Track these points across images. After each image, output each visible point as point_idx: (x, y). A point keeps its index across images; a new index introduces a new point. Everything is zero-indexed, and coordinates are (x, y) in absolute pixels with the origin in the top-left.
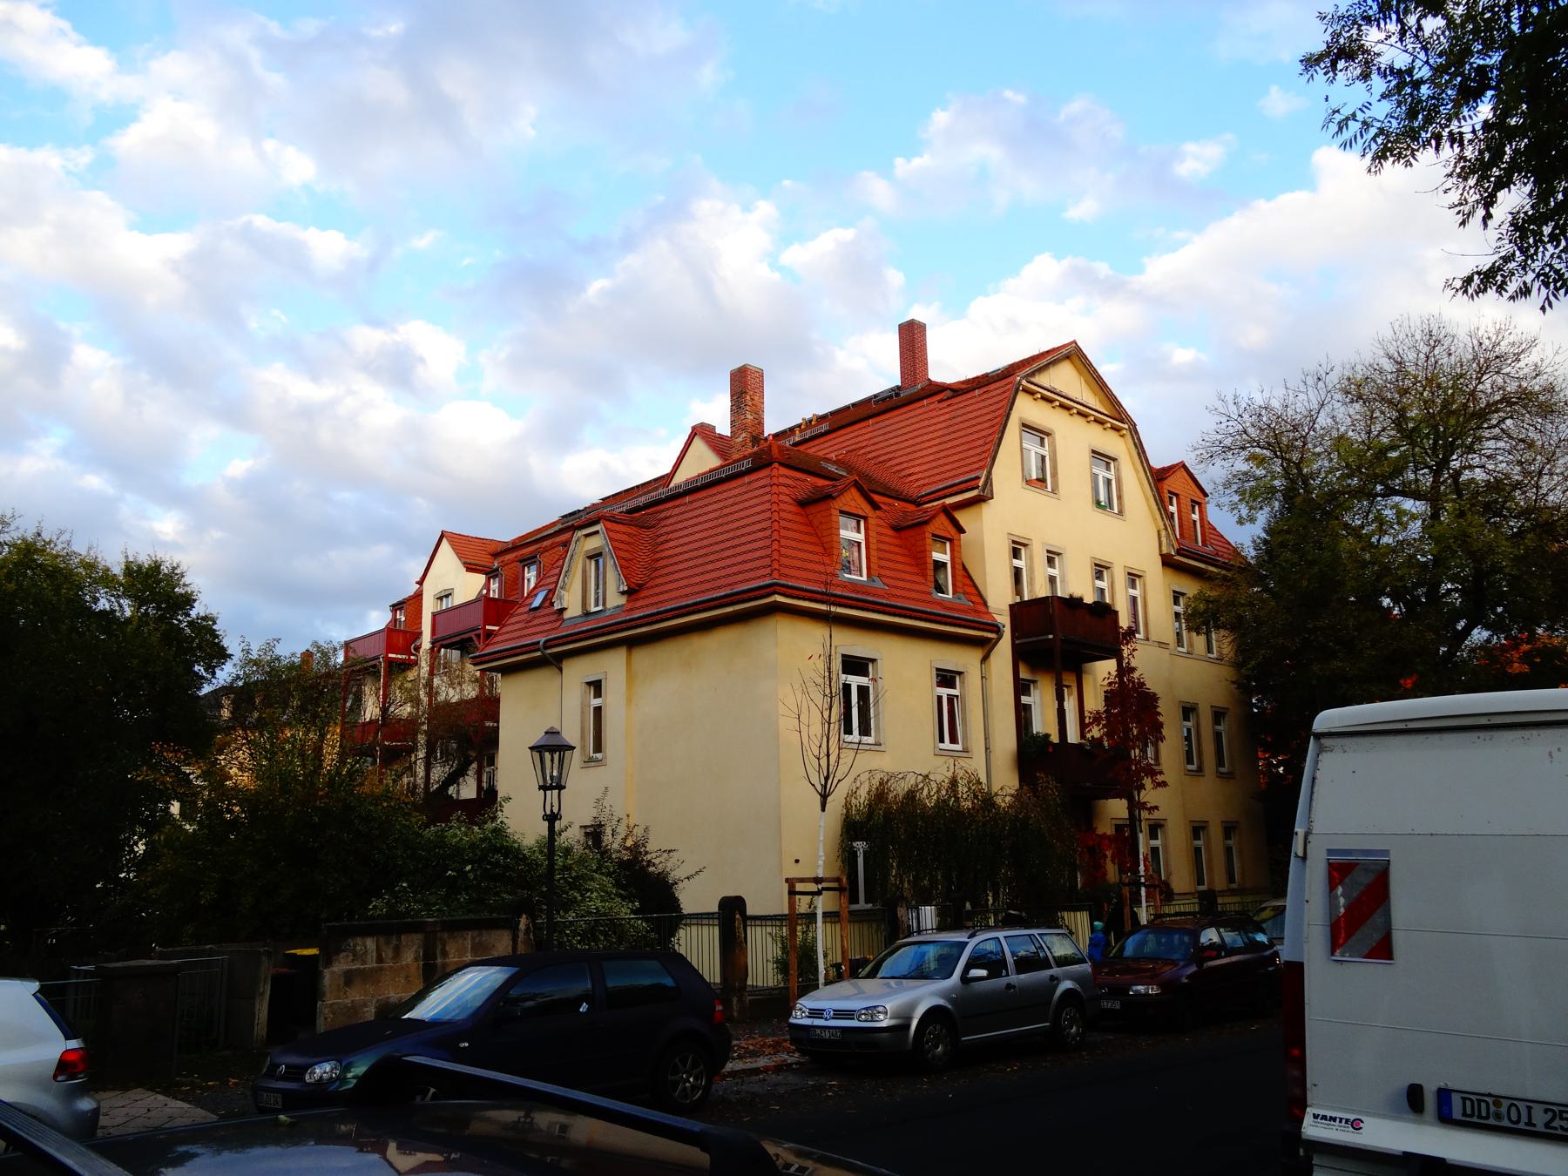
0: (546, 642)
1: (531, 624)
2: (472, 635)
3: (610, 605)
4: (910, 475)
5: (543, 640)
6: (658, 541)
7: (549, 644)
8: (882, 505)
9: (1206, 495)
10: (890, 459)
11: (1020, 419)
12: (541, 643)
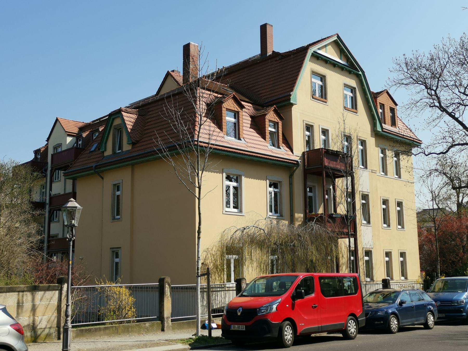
0: (96, 166)
1: (90, 158)
2: (69, 164)
3: (125, 149)
4: (261, 94)
5: (95, 165)
6: (146, 122)
7: (97, 167)
8: (245, 106)
9: (396, 105)
10: (253, 87)
11: (311, 69)
12: (94, 167)
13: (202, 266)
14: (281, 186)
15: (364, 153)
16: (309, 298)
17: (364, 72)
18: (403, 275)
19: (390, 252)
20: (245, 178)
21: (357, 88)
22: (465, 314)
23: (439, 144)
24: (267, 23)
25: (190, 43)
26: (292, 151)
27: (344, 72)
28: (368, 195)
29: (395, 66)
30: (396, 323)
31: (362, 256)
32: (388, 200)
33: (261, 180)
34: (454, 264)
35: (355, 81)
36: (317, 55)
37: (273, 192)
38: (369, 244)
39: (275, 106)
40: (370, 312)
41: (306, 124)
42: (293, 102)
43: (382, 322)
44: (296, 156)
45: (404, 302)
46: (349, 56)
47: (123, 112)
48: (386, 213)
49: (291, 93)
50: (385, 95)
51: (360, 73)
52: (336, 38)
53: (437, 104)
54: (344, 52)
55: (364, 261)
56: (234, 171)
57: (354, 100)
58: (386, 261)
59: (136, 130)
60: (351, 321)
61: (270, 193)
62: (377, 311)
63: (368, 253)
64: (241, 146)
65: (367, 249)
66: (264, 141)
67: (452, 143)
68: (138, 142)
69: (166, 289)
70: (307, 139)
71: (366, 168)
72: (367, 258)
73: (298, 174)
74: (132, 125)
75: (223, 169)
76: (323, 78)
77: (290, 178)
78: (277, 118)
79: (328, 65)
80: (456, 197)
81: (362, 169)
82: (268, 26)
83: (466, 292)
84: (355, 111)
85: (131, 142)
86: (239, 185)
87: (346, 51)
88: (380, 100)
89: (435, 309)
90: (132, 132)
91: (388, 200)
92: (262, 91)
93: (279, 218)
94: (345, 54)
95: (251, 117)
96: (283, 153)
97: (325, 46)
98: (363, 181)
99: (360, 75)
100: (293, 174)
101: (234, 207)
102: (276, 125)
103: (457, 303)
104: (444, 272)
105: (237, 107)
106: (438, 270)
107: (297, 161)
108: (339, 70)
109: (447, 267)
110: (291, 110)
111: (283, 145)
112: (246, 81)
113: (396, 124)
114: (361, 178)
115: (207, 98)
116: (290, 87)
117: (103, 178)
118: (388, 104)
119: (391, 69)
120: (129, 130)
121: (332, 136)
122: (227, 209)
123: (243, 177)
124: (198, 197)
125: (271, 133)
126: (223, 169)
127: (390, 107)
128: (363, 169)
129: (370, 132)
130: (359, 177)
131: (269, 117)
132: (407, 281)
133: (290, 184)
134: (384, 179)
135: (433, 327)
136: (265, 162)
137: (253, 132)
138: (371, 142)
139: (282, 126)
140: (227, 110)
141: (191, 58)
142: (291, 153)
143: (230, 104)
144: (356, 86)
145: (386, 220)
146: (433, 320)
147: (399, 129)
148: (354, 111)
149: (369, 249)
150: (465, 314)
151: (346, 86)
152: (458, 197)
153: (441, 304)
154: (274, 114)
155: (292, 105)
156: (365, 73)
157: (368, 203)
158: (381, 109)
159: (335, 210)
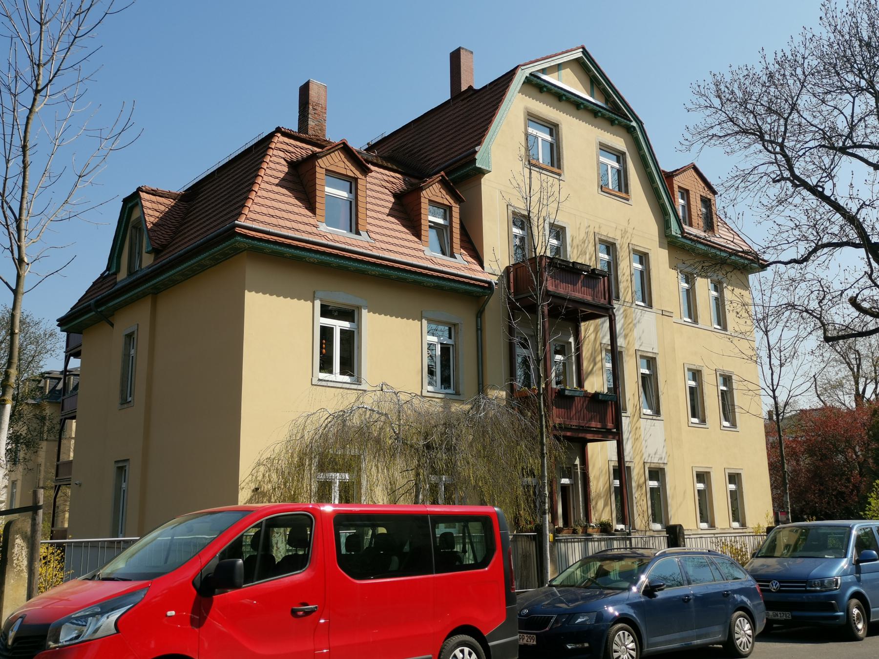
4: (429, 160)
9: (714, 192)
11: (526, 108)
13: (252, 497)
14: (458, 333)
15: (645, 277)
16: (547, 563)
17: (641, 122)
18: (736, 518)
19: (706, 472)
20: (369, 312)
21: (627, 154)
22: (841, 613)
23: (789, 243)
24: (462, 46)
25: (309, 81)
26: (481, 265)
27: (598, 121)
28: (655, 358)
29: (694, 98)
30: (632, 645)
31: (642, 480)
32: (701, 371)
33: (408, 319)
34: (843, 498)
35: (622, 140)
36: (542, 82)
37: (439, 345)
38: (658, 456)
39: (442, 173)
40: (555, 616)
41: (514, 213)
42: (483, 165)
43: (586, 645)
44: (489, 273)
45: (661, 586)
46: (610, 90)
47: (143, 191)
48: (695, 397)
49: (477, 148)
50: (692, 172)
51: (634, 124)
52: (581, 55)
53: (787, 174)
54: (599, 83)
55: (648, 490)
56: (342, 297)
57: (622, 177)
58: (730, 491)
59: (166, 227)
60: (462, 651)
61: (431, 346)
62: (575, 614)
63: (656, 473)
64: (350, 245)
65: (653, 466)
66: (417, 240)
67: (816, 242)
68: (164, 247)
69: (16, 550)
70: (517, 242)
71: (650, 306)
72: (654, 484)
73: (496, 309)
74: (158, 217)
75: (314, 292)
76: (553, 128)
77: (477, 317)
78: (448, 197)
79: (563, 105)
80: (853, 383)
81: (639, 307)
82: (462, 52)
83: (845, 557)
84: (624, 195)
85: (151, 248)
86: (356, 327)
87: (603, 81)
88: (678, 181)
89: (756, 603)
90: (156, 229)
91: (701, 371)
92: (432, 156)
93: (449, 397)
94: (601, 87)
95: (395, 195)
96: (459, 266)
97: (559, 67)
98: (643, 332)
99: (634, 127)
100: (484, 309)
101: (343, 372)
102: (447, 211)
103: (822, 584)
104: (823, 513)
105: (353, 169)
106: (787, 505)
107: (490, 283)
108: (589, 117)
109: (828, 503)
110: (480, 184)
111: (462, 251)
112: (410, 145)
113: (716, 228)
114: (638, 326)
115: (293, 152)
116: (476, 138)
117: (112, 325)
118: (697, 190)
119: (690, 106)
120: (149, 226)
121: (572, 240)
122: (323, 376)
123: (364, 312)
124: (14, 288)
125: (435, 226)
126: (314, 292)
127: (701, 195)
128: (641, 308)
129: (657, 239)
130: (634, 322)
131: (430, 195)
132: (744, 531)
133: (477, 330)
134: (690, 331)
135: (750, 653)
136: (415, 282)
137: (393, 223)
138: (660, 258)
139: (461, 214)
140: (329, 172)
141: (311, 107)
142: (479, 268)
143: (337, 160)
144: (626, 149)
145: (697, 409)
146: (749, 632)
147: (722, 237)
148: (621, 195)
149: (658, 465)
150: (841, 613)
151: (605, 148)
152: (857, 383)
153: (781, 586)
154: (441, 190)
155: (481, 172)
156: (644, 125)
157: (655, 375)
158: (683, 198)
159: (580, 383)
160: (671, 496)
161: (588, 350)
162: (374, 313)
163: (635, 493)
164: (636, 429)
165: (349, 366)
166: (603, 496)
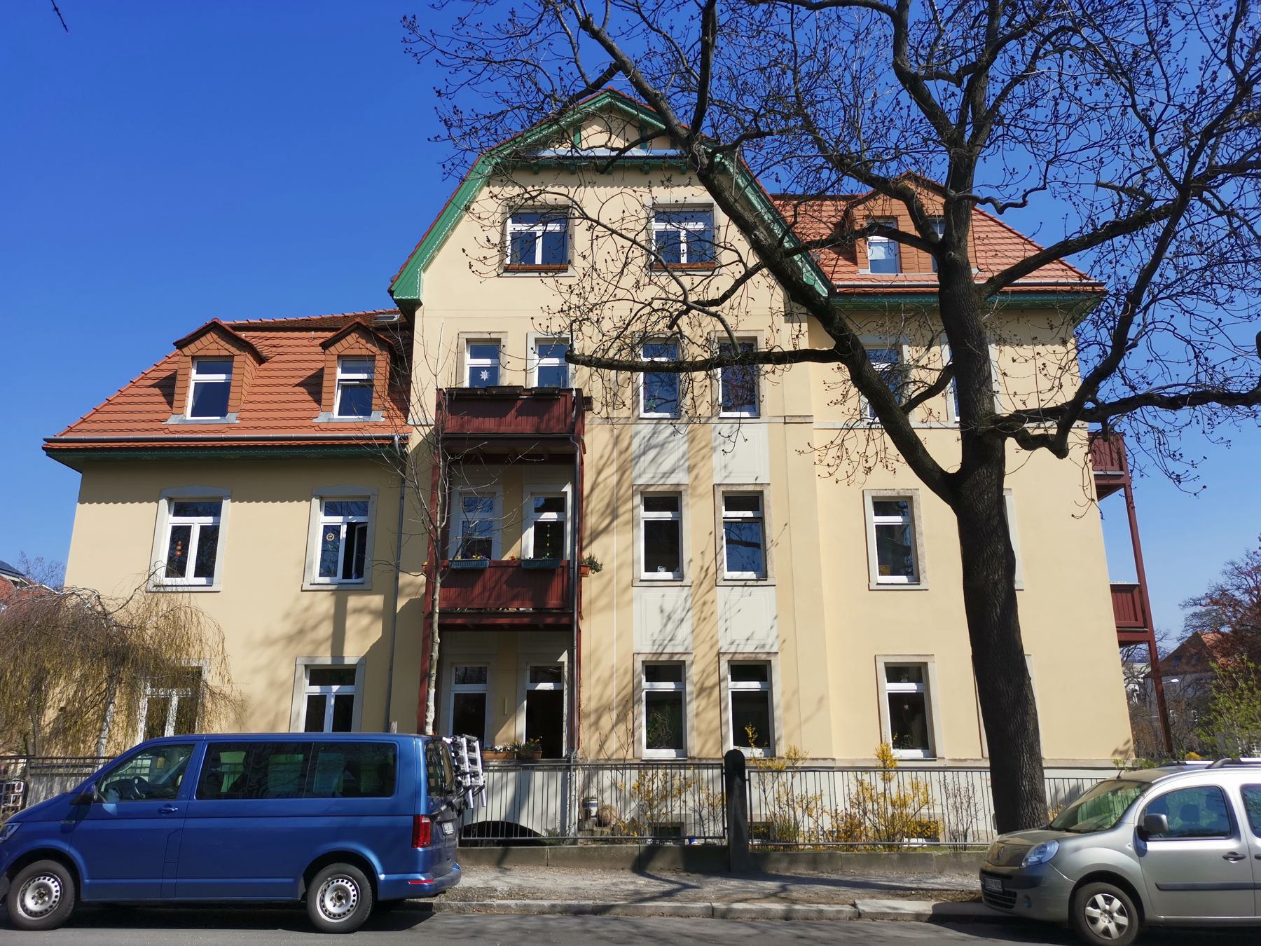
56: (194, 489)
101: (198, 574)
105: (228, 346)
160: (782, 705)
161: (602, 499)
162: (299, 501)
163: (691, 701)
164: (704, 604)
165: (206, 568)
166: (617, 707)
